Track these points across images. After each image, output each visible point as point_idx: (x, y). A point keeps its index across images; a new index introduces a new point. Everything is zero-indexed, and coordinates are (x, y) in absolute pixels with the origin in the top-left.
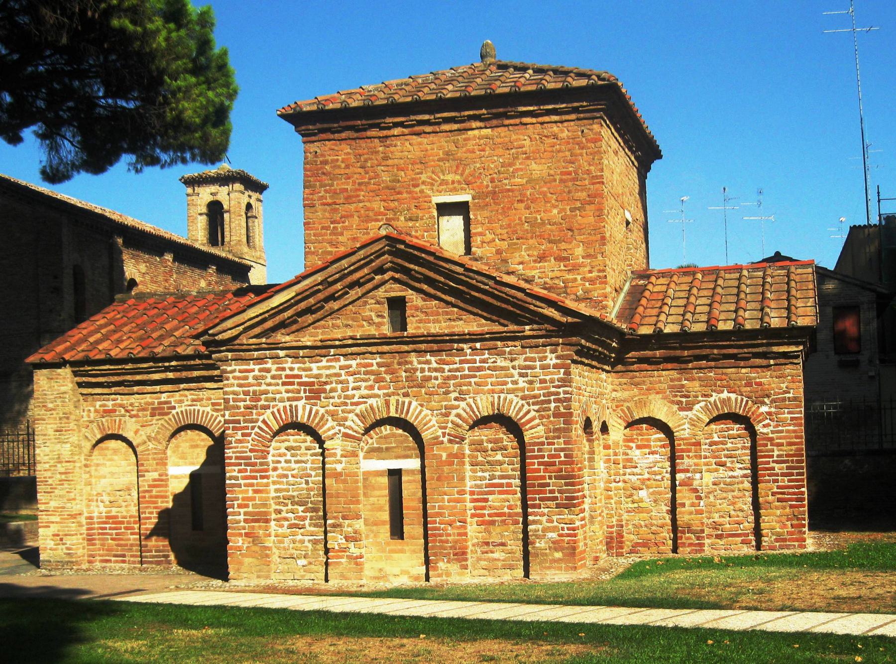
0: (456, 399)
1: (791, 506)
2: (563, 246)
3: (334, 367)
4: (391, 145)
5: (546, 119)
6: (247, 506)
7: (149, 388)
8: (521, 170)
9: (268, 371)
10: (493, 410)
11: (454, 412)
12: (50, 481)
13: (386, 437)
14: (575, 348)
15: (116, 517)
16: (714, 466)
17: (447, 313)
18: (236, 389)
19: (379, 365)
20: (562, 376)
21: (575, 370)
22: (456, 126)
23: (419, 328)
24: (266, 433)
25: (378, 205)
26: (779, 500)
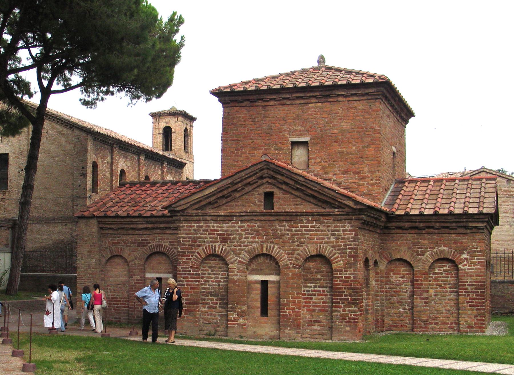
0: (298, 246)
2: (358, 166)
3: (235, 227)
4: (268, 110)
5: (351, 99)
6: (188, 296)
7: (137, 232)
9: (201, 227)
10: (317, 252)
11: (296, 252)
13: (260, 264)
14: (361, 222)
15: (117, 298)
16: (435, 286)
18: (184, 235)
19: (259, 226)
20: (353, 236)
21: (359, 233)
22: (302, 101)
23: (280, 208)
24: (199, 259)
26: (470, 306)
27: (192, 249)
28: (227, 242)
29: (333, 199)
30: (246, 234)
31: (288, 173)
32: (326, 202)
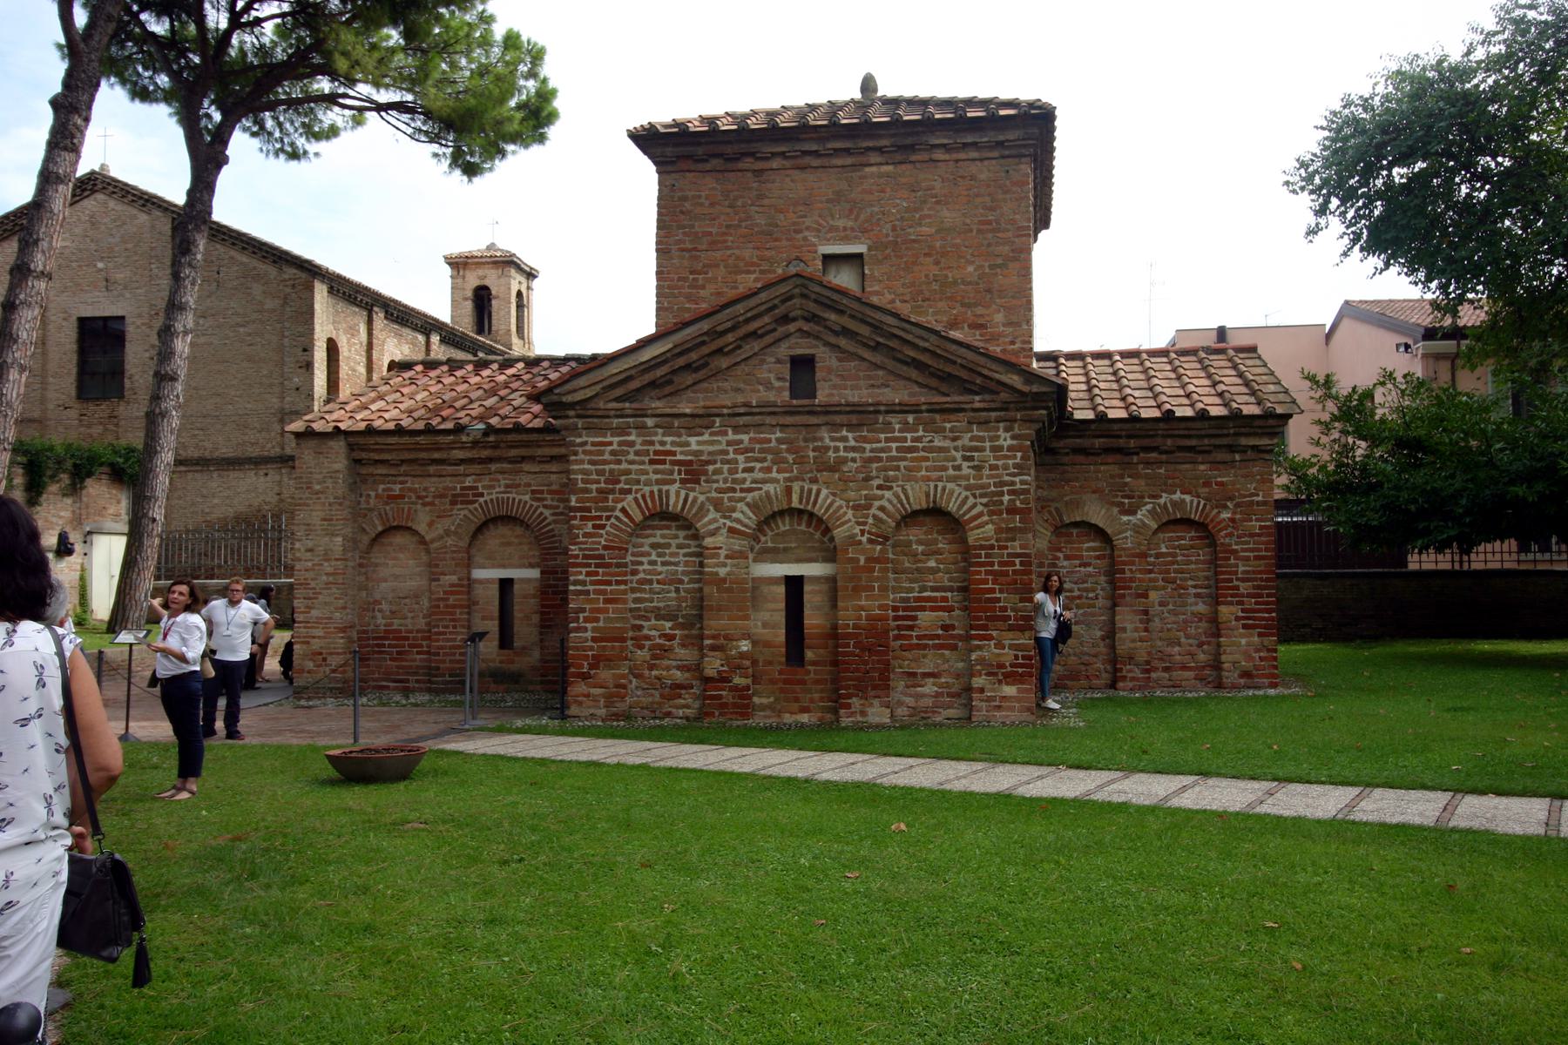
0: (880, 487)
1: (1260, 635)
2: (979, 310)
5: (962, 156)
6: (597, 620)
8: (929, 216)
9: (632, 444)
11: (877, 503)
12: (313, 584)
16: (1161, 583)
17: (870, 377)
19: (779, 441)
22: (849, 161)
25: (748, 253)
26: (1245, 627)
27: (607, 499)
28: (697, 482)
29: (971, 370)
30: (748, 460)
31: (856, 305)
32: (947, 378)
